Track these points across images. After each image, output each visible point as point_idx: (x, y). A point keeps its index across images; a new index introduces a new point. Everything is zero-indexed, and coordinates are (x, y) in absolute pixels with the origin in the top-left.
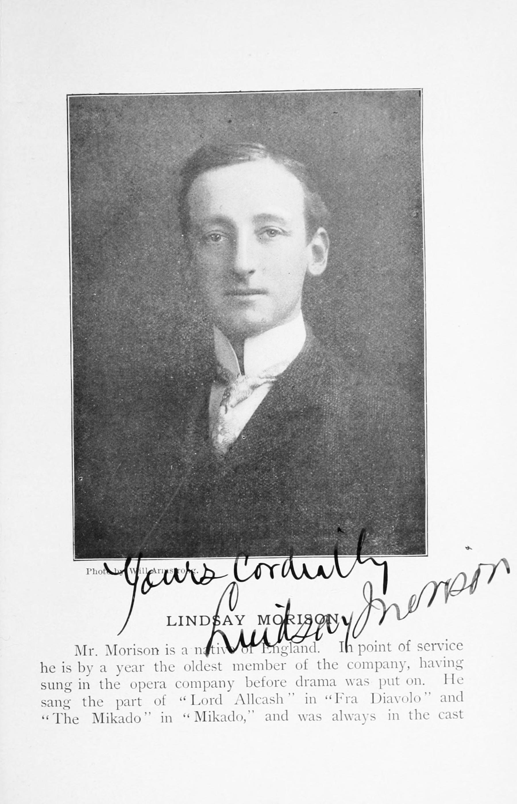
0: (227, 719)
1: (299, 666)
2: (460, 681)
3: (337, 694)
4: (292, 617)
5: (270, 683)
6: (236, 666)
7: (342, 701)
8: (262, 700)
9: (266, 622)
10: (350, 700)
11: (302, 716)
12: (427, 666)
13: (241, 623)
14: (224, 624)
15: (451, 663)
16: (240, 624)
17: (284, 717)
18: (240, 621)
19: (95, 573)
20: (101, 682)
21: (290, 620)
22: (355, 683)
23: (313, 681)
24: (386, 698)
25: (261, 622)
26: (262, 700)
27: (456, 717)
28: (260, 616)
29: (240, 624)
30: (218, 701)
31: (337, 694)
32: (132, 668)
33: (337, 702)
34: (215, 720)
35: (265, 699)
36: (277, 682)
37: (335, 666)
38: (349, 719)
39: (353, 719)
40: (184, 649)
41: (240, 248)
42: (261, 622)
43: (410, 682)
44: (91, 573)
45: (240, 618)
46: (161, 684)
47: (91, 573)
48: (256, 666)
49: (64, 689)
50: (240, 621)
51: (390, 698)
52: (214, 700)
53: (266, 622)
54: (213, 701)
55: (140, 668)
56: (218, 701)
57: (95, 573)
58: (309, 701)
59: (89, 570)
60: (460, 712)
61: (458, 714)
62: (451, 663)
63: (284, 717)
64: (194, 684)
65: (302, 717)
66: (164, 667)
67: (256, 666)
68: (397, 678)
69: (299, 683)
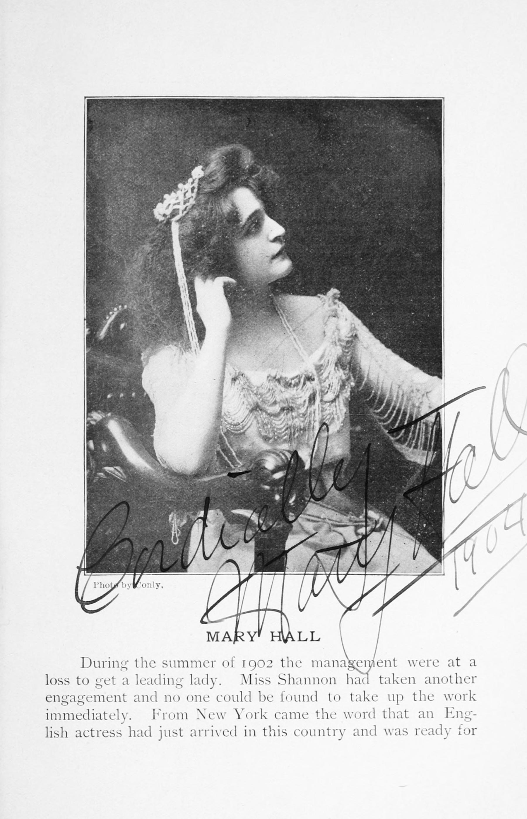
0: (143, 734)
1: (226, 664)
2: (374, 698)
3: (447, 708)
4: (241, 634)
5: (289, 698)
6: (315, 663)
7: (159, 718)
8: (281, 715)
9: (215, 639)
10: (166, 716)
11: (387, 731)
12: (354, 683)
13: (253, 639)
14: (223, 641)
15: (171, 681)
16: (252, 640)
17: (148, 733)
18: (252, 638)
19: (102, 586)
20: (414, 694)
21: (240, 637)
22: (393, 733)
23: (73, 697)
24: (95, 714)
25: (210, 639)
26: (281, 715)
27: (175, 735)
28: (209, 633)
29: (252, 640)
30: (372, 715)
31: (447, 708)
32: (147, 681)
33: (154, 718)
34: (263, 717)
35: (99, 715)
36: (366, 714)
37: (206, 699)
38: (389, 734)
39: (393, 734)
40: (473, 661)
41: (224, 340)
42: (210, 639)
43: (190, 698)
44: (98, 586)
45: (252, 634)
46: (71, 698)
47: (98, 586)
48: (97, 698)
49: (61, 702)
50: (252, 638)
51: (99, 715)
52: (368, 714)
53: (215, 639)
54: (367, 715)
55: (429, 681)
56: (372, 715)
57: (102, 586)
58: (248, 734)
59: (96, 584)
60: (180, 730)
61: (178, 732)
62: (171, 681)
63: (148, 733)
64: (180, 715)
65: (388, 732)
66: (423, 697)
67: (97, 698)
68: (124, 695)
69: (400, 698)
